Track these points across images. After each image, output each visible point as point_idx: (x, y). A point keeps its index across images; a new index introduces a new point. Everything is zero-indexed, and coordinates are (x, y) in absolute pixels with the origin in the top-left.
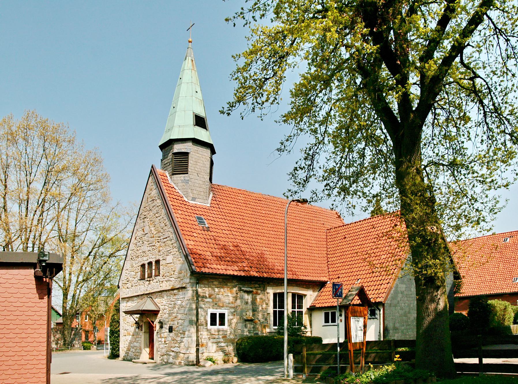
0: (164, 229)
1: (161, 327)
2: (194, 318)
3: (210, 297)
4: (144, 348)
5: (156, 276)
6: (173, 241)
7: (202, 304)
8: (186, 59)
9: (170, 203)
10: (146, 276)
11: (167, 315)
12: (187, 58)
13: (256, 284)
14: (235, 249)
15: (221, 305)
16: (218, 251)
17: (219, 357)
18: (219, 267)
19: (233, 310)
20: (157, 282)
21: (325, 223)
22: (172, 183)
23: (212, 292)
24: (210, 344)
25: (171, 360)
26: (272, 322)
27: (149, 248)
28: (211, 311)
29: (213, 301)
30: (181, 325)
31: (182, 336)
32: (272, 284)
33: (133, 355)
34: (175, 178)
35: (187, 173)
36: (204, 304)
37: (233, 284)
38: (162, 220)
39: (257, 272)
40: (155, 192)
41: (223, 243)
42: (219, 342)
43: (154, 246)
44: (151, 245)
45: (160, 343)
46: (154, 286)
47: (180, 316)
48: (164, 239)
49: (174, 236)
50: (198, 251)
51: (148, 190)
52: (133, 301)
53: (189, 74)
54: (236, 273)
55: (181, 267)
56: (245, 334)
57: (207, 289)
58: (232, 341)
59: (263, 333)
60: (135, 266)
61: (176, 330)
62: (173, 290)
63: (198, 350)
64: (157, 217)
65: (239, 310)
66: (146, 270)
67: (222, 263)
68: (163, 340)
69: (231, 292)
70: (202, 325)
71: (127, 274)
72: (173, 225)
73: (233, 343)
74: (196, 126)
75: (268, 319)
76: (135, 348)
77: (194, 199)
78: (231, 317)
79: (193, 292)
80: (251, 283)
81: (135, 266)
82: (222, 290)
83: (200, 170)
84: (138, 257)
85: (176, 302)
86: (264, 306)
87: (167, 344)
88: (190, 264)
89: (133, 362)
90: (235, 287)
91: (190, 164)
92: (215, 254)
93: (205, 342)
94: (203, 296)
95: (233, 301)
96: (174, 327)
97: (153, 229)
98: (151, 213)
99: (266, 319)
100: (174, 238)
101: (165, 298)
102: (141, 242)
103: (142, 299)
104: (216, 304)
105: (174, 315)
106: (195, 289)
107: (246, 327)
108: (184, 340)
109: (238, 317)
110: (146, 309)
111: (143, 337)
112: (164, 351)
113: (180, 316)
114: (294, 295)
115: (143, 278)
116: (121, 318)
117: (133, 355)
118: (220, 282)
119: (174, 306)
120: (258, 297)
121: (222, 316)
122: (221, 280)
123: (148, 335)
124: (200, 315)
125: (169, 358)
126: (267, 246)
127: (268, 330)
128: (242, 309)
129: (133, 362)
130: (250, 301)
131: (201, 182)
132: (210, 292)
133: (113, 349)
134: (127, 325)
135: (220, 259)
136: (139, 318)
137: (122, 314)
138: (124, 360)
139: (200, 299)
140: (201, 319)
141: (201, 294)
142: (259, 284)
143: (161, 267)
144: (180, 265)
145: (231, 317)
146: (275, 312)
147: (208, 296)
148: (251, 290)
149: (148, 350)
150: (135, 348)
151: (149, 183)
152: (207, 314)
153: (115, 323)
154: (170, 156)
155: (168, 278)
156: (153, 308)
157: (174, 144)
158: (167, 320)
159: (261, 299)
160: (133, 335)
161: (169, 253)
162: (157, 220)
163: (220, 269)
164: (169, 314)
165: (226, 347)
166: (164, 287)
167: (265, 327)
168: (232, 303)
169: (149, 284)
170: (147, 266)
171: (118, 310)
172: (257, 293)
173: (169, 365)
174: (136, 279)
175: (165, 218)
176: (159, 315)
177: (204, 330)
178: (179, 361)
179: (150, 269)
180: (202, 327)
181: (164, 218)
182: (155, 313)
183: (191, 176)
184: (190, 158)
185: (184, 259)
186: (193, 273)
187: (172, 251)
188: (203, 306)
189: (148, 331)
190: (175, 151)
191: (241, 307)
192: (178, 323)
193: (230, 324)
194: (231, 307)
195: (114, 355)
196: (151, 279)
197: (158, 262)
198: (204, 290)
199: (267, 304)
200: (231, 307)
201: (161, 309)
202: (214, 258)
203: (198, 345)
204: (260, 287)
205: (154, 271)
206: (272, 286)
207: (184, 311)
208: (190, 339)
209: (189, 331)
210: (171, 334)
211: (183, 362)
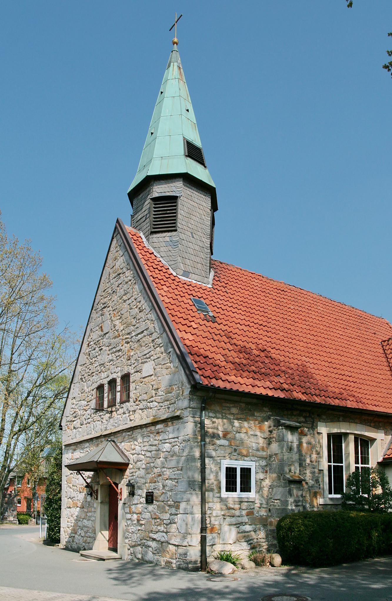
0: (138, 317)
1: (132, 494)
2: (198, 477)
3: (225, 436)
4: (101, 530)
5: (122, 402)
6: (155, 335)
7: (210, 450)
8: (169, 66)
9: (148, 274)
10: (106, 405)
11: (142, 472)
12: (172, 64)
13: (300, 415)
14: (262, 354)
15: (244, 452)
16: (235, 355)
17: (241, 551)
18: (239, 379)
19: (264, 463)
20: (124, 413)
21: (376, 332)
22: (150, 248)
23: (227, 426)
24: (226, 528)
25: (150, 556)
26: (327, 487)
27: (110, 357)
28: (226, 463)
29: (230, 445)
30: (171, 490)
31: (173, 511)
32: (324, 417)
33: (81, 541)
34: (155, 240)
35: (176, 230)
36: (215, 450)
37: (264, 415)
38: (134, 303)
39: (303, 393)
40: (120, 261)
41: (242, 344)
42: (241, 524)
43: (119, 351)
44: (114, 350)
45: (129, 522)
46: (120, 420)
47: (168, 473)
48: (137, 335)
49: (157, 325)
50: (202, 351)
51: (109, 261)
52: (83, 449)
53: (174, 87)
54: (270, 393)
55: (171, 380)
56: (290, 508)
57: (220, 420)
58: (264, 522)
59: (314, 507)
60: (87, 390)
61: (161, 499)
62: (154, 423)
63: (203, 540)
64: (125, 301)
65: (275, 463)
66: (106, 395)
67: (245, 374)
68: (135, 516)
69: (260, 428)
70: (212, 490)
71: (73, 406)
72: (156, 305)
73: (265, 526)
74: (189, 159)
75: (320, 480)
76: (86, 529)
77: (186, 274)
78: (261, 476)
79: (196, 426)
80: (292, 415)
81: (87, 390)
82: (246, 424)
83: (195, 228)
84: (91, 375)
85: (160, 447)
86: (314, 456)
87: (142, 525)
88: (189, 372)
89: (82, 555)
90: (267, 419)
91: (179, 216)
92: (231, 359)
93: (217, 523)
94: (214, 434)
95: (265, 445)
96: (156, 493)
97: (117, 323)
98: (115, 298)
99: (317, 481)
100: (157, 329)
101: (140, 440)
102: (97, 349)
103: (98, 445)
104: (235, 450)
105: (156, 470)
106: (198, 419)
107: (290, 493)
108: (179, 518)
109: (274, 475)
110: (105, 460)
111: (98, 511)
112: (135, 537)
113: (168, 473)
114: (357, 438)
115: (99, 408)
116: (64, 478)
117: (81, 541)
118: (242, 410)
119: (157, 455)
120: (304, 440)
121: (246, 473)
122: (243, 405)
123: (106, 508)
124: (207, 471)
125: (146, 553)
126: (307, 355)
127: (321, 501)
128: (282, 460)
129: (82, 555)
130: (295, 445)
131: (197, 248)
132: (226, 426)
133: (50, 529)
134: (74, 488)
135: (240, 368)
136: (93, 478)
137: (65, 471)
138: (66, 549)
139: (207, 440)
140: (211, 478)
141: (210, 431)
142: (305, 417)
143: (132, 386)
144: (168, 377)
145: (261, 476)
146: (330, 467)
147: (221, 435)
148: (113, 485)
149: (106, 533)
150: (86, 529)
151: (111, 249)
152: (220, 468)
153: (54, 485)
154: (148, 204)
155: (144, 403)
156: (116, 458)
157: (152, 185)
158: (143, 481)
159: (309, 443)
160: (82, 507)
161: (147, 358)
162: (126, 305)
163: (244, 384)
164: (146, 469)
165: (253, 533)
166: (137, 420)
167: (315, 495)
168: (263, 449)
169: (110, 418)
170: (106, 388)
171: (59, 466)
172: (303, 434)
173: (147, 568)
174: (88, 412)
175: (141, 298)
176: (128, 472)
177: (216, 500)
178: (167, 558)
179: (113, 392)
180: (211, 494)
181: (138, 300)
182: (120, 468)
183: (182, 236)
184: (180, 206)
185: (177, 362)
186: (196, 388)
187: (152, 353)
188: (214, 454)
189: (107, 500)
190: (155, 195)
191: (280, 457)
192: (164, 486)
193: (260, 490)
194: (262, 458)
195: (52, 540)
196: (114, 409)
197: (126, 378)
198: (215, 424)
199: (318, 453)
200: (262, 458)
201: (131, 462)
202: (231, 366)
203: (203, 529)
204: (306, 422)
205: (118, 394)
206: (325, 421)
207: (178, 462)
208: (189, 517)
209: (188, 501)
210: (151, 507)
211: (174, 561)
